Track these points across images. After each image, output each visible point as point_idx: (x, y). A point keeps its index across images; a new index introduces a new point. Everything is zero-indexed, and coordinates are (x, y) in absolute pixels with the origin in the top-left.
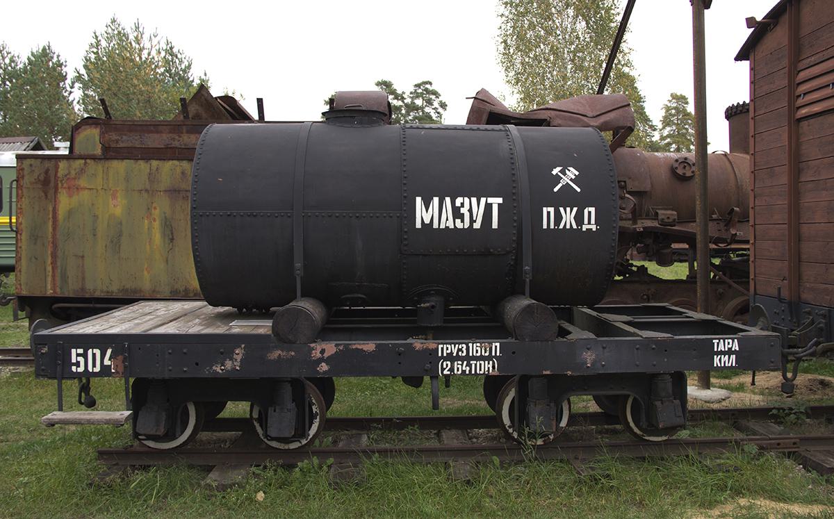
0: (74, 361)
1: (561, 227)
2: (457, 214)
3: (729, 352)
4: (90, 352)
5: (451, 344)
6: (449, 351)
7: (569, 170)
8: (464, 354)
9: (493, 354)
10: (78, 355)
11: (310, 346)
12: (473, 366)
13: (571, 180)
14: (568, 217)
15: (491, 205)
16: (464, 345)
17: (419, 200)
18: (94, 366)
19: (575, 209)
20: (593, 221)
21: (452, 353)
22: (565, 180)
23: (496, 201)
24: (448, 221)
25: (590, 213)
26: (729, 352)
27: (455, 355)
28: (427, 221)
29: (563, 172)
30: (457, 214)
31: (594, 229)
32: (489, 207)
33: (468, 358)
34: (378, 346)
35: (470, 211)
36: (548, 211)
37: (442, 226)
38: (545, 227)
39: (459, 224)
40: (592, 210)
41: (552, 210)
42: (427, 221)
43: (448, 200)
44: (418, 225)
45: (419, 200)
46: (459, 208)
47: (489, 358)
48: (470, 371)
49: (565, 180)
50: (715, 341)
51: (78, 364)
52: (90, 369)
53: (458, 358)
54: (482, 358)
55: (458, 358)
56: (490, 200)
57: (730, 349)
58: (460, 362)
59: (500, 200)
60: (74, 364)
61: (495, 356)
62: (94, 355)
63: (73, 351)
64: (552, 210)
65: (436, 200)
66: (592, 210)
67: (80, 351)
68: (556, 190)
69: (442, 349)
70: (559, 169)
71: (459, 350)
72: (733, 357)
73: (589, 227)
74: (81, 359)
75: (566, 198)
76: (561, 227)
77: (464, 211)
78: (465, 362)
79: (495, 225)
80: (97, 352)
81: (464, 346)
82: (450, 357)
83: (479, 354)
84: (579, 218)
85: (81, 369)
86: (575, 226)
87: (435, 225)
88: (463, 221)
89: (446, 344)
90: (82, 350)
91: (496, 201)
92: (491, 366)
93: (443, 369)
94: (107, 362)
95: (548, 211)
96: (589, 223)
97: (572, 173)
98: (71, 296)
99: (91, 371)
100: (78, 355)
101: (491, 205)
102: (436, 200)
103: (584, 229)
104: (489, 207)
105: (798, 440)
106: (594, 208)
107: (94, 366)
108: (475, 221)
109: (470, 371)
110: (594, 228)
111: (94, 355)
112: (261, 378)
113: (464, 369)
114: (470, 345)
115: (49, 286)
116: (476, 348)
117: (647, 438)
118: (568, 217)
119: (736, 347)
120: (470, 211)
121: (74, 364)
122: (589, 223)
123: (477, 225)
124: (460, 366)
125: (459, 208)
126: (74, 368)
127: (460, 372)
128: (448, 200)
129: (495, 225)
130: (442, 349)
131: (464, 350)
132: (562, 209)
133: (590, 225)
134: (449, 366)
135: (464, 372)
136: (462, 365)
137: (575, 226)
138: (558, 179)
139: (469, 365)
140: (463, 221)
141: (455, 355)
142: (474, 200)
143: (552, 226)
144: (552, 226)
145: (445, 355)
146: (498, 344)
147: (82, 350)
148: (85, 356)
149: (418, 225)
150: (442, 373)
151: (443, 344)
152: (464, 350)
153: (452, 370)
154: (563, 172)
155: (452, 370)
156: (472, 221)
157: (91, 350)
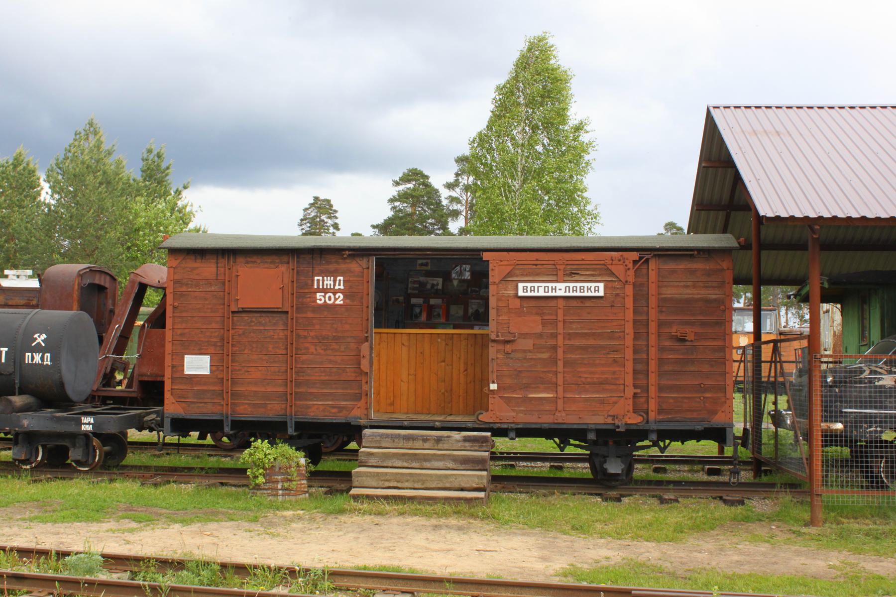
3: (89, 424)
11: (10, 402)
13: (42, 340)
19: (41, 354)
22: (39, 340)
25: (47, 356)
26: (89, 424)
29: (39, 336)
34: (115, 388)
36: (28, 355)
38: (27, 362)
40: (49, 355)
49: (39, 340)
50: (83, 418)
57: (89, 422)
59: (6, 349)
66: (49, 355)
68: (33, 345)
70: (38, 334)
72: (91, 426)
74: (323, 299)
75: (38, 349)
76: (34, 362)
84: (42, 359)
95: (28, 355)
96: (47, 361)
97: (44, 336)
98: (825, 304)
105: (696, 252)
110: (49, 363)
112: (877, 217)
115: (765, 308)
117: (79, 468)
118: (37, 358)
119: (92, 421)
122: (47, 361)
132: (34, 354)
133: (47, 362)
137: (40, 362)
138: (36, 339)
143: (30, 362)
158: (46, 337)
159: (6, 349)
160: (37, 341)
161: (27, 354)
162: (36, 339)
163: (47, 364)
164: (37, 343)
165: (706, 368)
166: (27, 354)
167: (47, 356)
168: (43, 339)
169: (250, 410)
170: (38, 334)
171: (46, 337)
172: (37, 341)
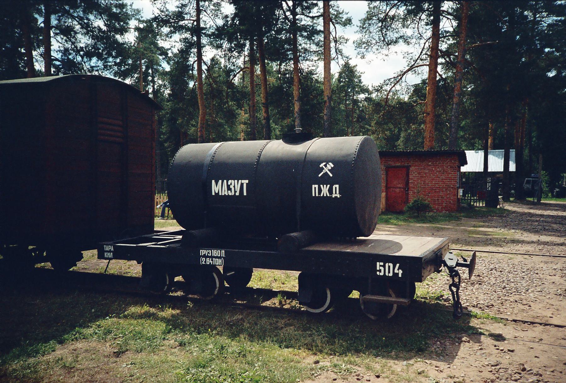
0: (378, 269)
1: (322, 195)
2: (229, 189)
3: (110, 251)
4: (387, 265)
5: (205, 250)
6: (204, 253)
7: (329, 164)
8: (210, 255)
9: (222, 256)
10: (380, 266)
12: (214, 260)
13: (329, 170)
14: (325, 190)
15: (243, 183)
16: (210, 251)
17: (213, 181)
18: (389, 272)
19: (328, 186)
20: (338, 192)
21: (205, 254)
22: (326, 170)
23: (246, 182)
24: (225, 192)
25: (336, 188)
26: (110, 251)
27: (206, 255)
28: (217, 192)
29: (326, 166)
30: (229, 189)
31: (339, 197)
32: (242, 184)
33: (212, 257)
35: (234, 187)
37: (223, 194)
38: (314, 195)
39: (230, 194)
40: (337, 186)
41: (317, 186)
42: (217, 192)
43: (225, 181)
44: (213, 194)
45: (213, 181)
46: (230, 185)
47: (220, 258)
48: (213, 263)
49: (326, 170)
51: (380, 271)
52: (387, 274)
53: (208, 257)
54: (217, 257)
55: (208, 257)
56: (243, 181)
57: (110, 250)
58: (209, 259)
59: (247, 181)
60: (378, 271)
61: (223, 257)
62: (389, 267)
63: (378, 263)
64: (317, 186)
65: (220, 181)
66: (337, 186)
67: (382, 264)
69: (202, 252)
70: (324, 163)
71: (208, 253)
72: (112, 254)
73: (336, 195)
74: (382, 268)
75: (325, 180)
76: (322, 195)
77: (232, 187)
78: (211, 259)
79: (245, 194)
80: (391, 265)
81: (210, 251)
82: (205, 256)
83: (216, 256)
84: (330, 191)
85: (382, 274)
86: (328, 195)
87: (220, 194)
88: (231, 192)
89: (203, 250)
90: (383, 263)
91: (246, 182)
92: (221, 261)
93: (202, 261)
94: (396, 271)
96: (336, 193)
99: (387, 275)
100: (380, 266)
101: (243, 183)
102: (220, 181)
103: (333, 197)
104: (242, 184)
106: (338, 185)
107: (389, 272)
108: (236, 192)
109: (213, 263)
111: (389, 267)
113: (396, 271)
114: (213, 251)
116: (216, 253)
118: (325, 190)
119: (112, 249)
120: (234, 187)
121: (378, 271)
122: (336, 193)
123: (237, 194)
124: (209, 260)
125: (230, 185)
126: (378, 273)
127: (209, 263)
128: (225, 181)
129: (245, 194)
130: (202, 252)
131: (210, 253)
132: (322, 186)
134: (204, 260)
135: (210, 263)
136: (210, 260)
137: (328, 195)
138: (322, 169)
139: (212, 260)
140: (231, 192)
141: (206, 255)
142: (236, 181)
143: (317, 195)
144: (317, 195)
145: (203, 255)
146: (224, 251)
147: (383, 263)
148: (384, 266)
149: (213, 194)
150: (202, 263)
151: (202, 250)
152: (210, 253)
153: (205, 262)
154: (326, 166)
155: (205, 262)
156: (235, 192)
157: (387, 264)
158: (332, 166)
159: (247, 181)
160: (324, 172)
161: (313, 186)
162: (322, 169)
163: (336, 197)
164: (324, 173)
165: (437, 180)
166: (313, 186)
167: (336, 188)
168: (330, 168)
169: (330, 380)
170: (324, 163)
171: (332, 166)
172: (324, 172)
